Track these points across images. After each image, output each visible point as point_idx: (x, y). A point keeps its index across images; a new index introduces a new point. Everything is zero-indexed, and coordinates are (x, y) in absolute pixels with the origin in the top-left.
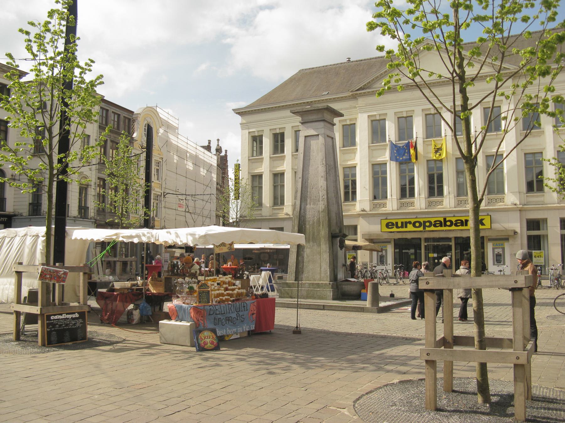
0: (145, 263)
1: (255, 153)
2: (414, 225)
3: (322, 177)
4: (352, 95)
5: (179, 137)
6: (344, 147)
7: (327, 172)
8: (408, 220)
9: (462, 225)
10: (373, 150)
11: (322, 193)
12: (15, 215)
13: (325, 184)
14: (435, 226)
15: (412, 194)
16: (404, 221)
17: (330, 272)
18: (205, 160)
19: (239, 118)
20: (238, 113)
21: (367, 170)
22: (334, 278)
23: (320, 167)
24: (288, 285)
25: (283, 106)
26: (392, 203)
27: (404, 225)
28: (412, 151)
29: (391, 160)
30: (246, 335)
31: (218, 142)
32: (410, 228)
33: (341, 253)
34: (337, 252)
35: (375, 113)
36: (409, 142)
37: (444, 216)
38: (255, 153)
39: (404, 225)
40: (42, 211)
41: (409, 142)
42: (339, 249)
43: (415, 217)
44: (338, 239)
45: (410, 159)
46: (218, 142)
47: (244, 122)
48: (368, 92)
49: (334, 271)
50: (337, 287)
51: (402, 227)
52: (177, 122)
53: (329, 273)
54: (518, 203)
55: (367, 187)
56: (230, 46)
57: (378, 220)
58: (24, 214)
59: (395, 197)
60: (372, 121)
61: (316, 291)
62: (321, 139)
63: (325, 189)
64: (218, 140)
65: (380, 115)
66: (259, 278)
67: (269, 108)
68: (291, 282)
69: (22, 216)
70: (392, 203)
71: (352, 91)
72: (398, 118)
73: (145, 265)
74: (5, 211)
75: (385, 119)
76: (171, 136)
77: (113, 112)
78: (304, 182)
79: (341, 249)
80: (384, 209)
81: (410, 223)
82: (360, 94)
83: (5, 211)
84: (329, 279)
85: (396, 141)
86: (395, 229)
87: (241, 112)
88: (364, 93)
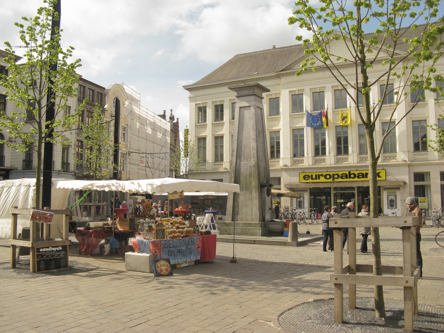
0: (114, 207)
1: (200, 120)
2: (325, 177)
3: (253, 139)
4: (277, 75)
5: (141, 108)
6: (270, 115)
7: (257, 136)
8: (320, 173)
10: (293, 118)
11: (253, 152)
12: (12, 170)
13: (256, 145)
14: (342, 178)
15: (324, 153)
16: (317, 174)
17: (260, 214)
18: (161, 126)
19: (188, 93)
20: (187, 89)
21: (289, 134)
22: (263, 219)
23: (252, 131)
24: (227, 224)
25: (222, 84)
26: (308, 160)
27: (318, 177)
28: (324, 119)
29: (307, 126)
30: (193, 263)
31: (171, 112)
32: (322, 179)
33: (268, 199)
34: (265, 199)
35: (295, 89)
36: (321, 112)
37: (349, 170)
38: (200, 120)
39: (318, 177)
40: (33, 166)
41: (321, 112)
42: (266, 196)
43: (326, 170)
44: (266, 188)
45: (322, 125)
46: (171, 112)
47: (192, 96)
48: (289, 73)
49: (263, 213)
50: (265, 226)
51: (316, 179)
52: (139, 96)
53: (258, 215)
54: (407, 160)
55: (289, 147)
56: (181, 36)
57: (297, 173)
58: (19, 169)
59: (310, 155)
60: (292, 95)
61: (249, 229)
62: (252, 109)
63: (256, 148)
64: (171, 110)
65: (299, 91)
66: (204, 219)
67: (211, 85)
68: (228, 222)
69: (17, 170)
70: (308, 160)
71: (276, 72)
72: (313, 93)
73: (114, 209)
74: (4, 166)
75: (302, 94)
76: (134, 107)
77: (89, 88)
78: (239, 144)
79: (268, 196)
80: (302, 164)
81: (322, 175)
82: (283, 74)
83: (4, 166)
84: (258, 220)
85: (311, 111)
86: (310, 180)
87: (189, 89)
88: (286, 73)
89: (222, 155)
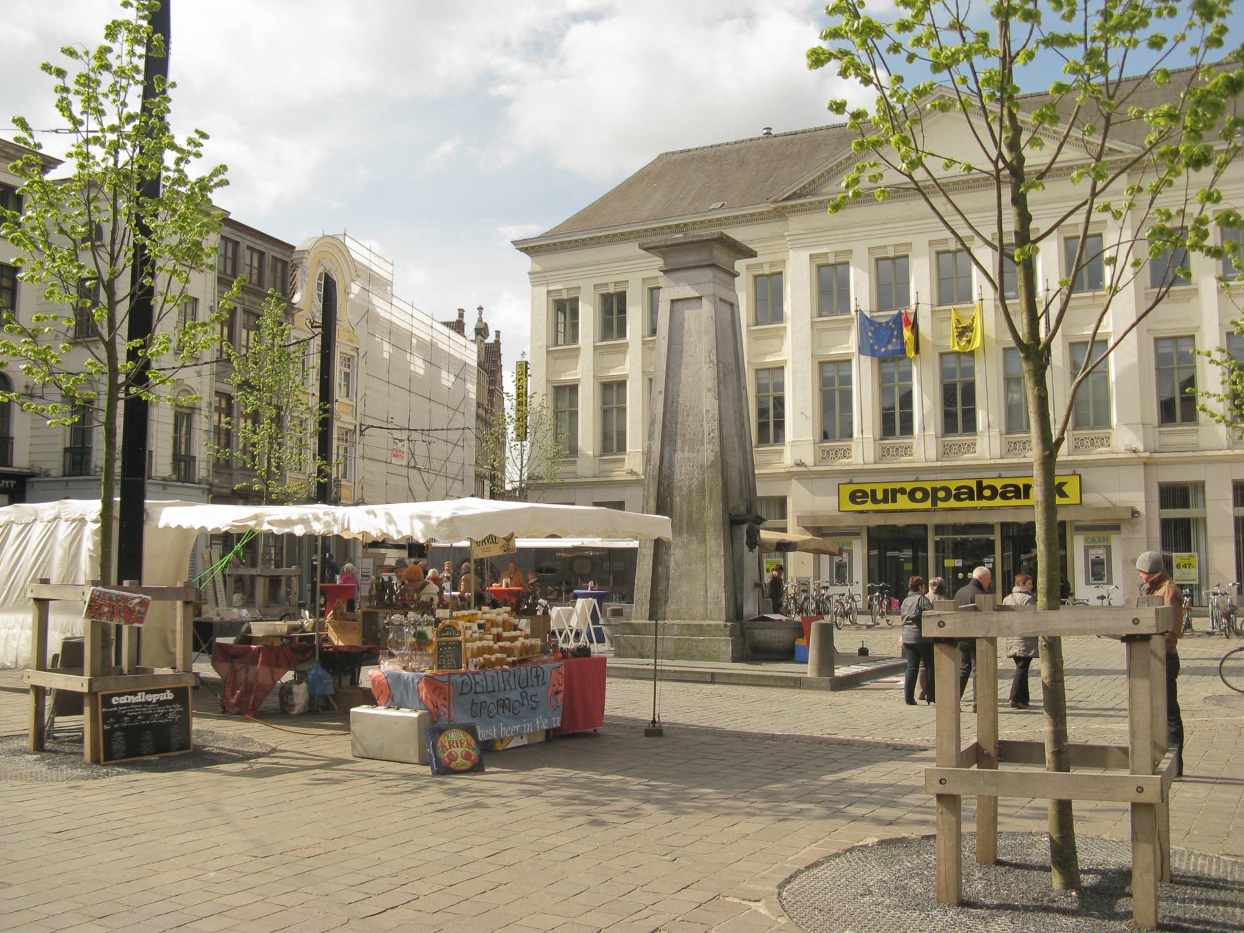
1: (561, 336)
2: (912, 496)
3: (709, 390)
4: (775, 209)
5: (395, 301)
6: (757, 324)
7: (721, 380)
8: (897, 486)
9: (1018, 496)
10: (821, 331)
11: (710, 426)
12: (33, 475)
13: (716, 407)
14: (957, 498)
15: (907, 429)
16: (889, 487)
17: (727, 601)
18: (452, 352)
19: (526, 259)
20: (525, 250)
21: (809, 375)
22: (736, 613)
23: (705, 368)
24: (635, 629)
25: (622, 234)
26: (863, 447)
27: (890, 495)
28: (907, 333)
29: (860, 352)
30: (541, 738)
31: (480, 314)
32: (903, 502)
33: (750, 558)
34: (742, 556)
35: (825, 250)
36: (900, 314)
37: (978, 475)
38: (561, 336)
39: (890, 495)
40: (93, 465)
41: (900, 314)
42: (746, 548)
43: (913, 478)
44: (745, 527)
45: (903, 351)
46: (480, 314)
47: (538, 268)
48: (811, 203)
49: (736, 598)
50: (743, 633)
51: (885, 500)
52: (390, 268)
53: (723, 602)
54: (1141, 448)
55: (809, 413)
56: (506, 101)
57: (832, 484)
58: (53, 473)
59: (869, 434)
60: (819, 267)
61: (697, 641)
62: (707, 307)
63: (716, 416)
64: (480, 309)
65: (836, 254)
66: (571, 613)
67: (591, 239)
68: (640, 621)
69: (48, 476)
70: (863, 447)
71: (775, 202)
72: (877, 260)
73: (319, 585)
74: (11, 466)
75: (847, 263)
76: (376, 301)
77: (248, 247)
78: (669, 402)
79: (751, 550)
80: (845, 461)
81: (903, 491)
82: (792, 206)
83: (11, 466)
84: (723, 616)
85: (871, 312)
86: (870, 506)
87: (530, 248)
88: (802, 205)
89: (622, 435)
